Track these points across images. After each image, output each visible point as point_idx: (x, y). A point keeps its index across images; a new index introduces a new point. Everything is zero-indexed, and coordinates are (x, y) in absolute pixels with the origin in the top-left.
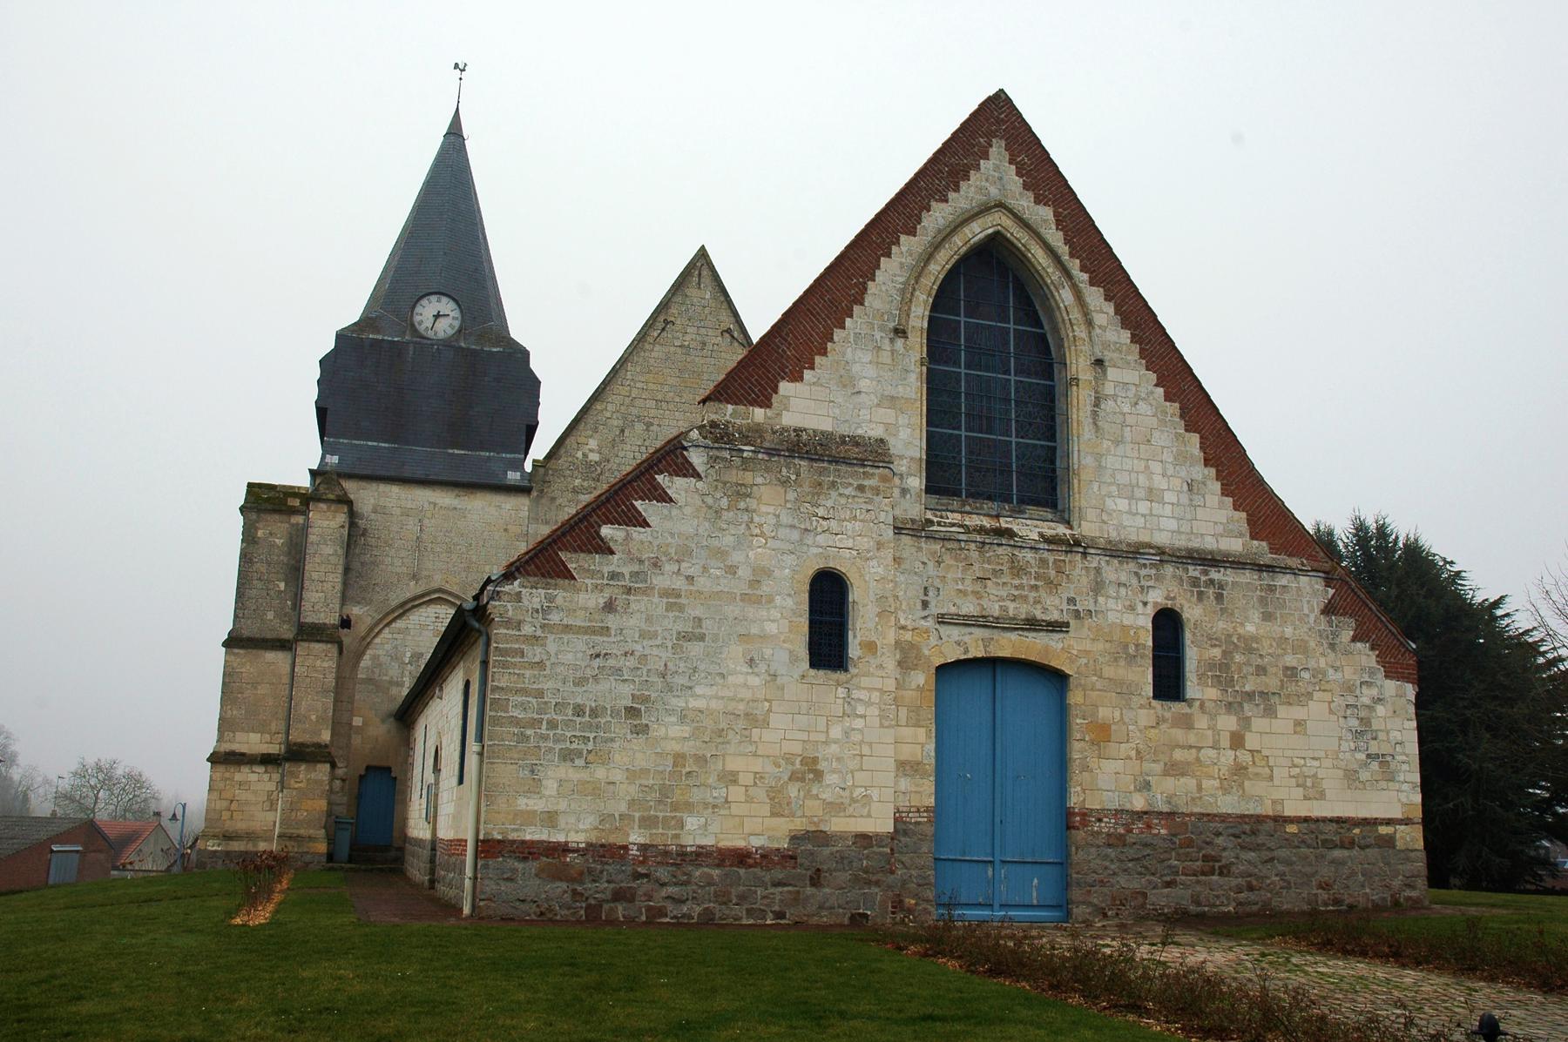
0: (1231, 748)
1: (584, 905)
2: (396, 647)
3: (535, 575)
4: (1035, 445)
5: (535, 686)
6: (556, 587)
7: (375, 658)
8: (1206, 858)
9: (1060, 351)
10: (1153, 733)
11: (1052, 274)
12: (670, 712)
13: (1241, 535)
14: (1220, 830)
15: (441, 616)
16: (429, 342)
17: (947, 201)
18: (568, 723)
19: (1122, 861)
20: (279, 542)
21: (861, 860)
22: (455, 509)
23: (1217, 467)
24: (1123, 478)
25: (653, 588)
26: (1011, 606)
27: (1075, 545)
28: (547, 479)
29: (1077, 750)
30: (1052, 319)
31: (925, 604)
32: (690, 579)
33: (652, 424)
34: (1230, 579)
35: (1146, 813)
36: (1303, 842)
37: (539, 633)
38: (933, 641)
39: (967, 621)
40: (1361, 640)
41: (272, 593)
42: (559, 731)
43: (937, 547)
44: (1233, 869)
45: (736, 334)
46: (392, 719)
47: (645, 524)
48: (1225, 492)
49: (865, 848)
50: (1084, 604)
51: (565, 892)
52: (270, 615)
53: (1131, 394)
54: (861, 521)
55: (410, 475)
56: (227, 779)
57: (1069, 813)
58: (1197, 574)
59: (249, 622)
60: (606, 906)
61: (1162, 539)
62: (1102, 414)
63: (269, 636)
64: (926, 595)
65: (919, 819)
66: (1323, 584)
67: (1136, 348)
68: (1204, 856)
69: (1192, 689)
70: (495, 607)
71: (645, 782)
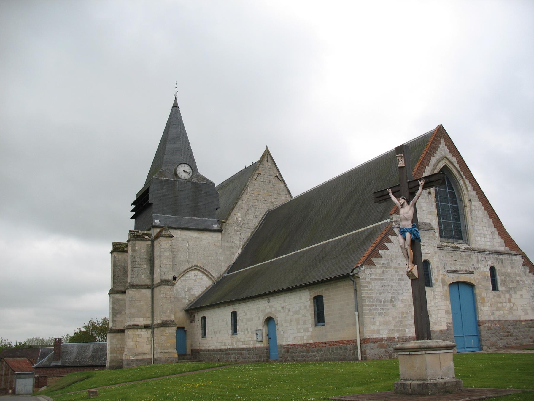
0: (509, 303)
1: (388, 354)
2: (183, 286)
3: (367, 265)
4: (456, 223)
5: (371, 295)
6: (372, 268)
7: (177, 290)
8: (508, 332)
9: (460, 197)
10: (493, 299)
11: (458, 176)
12: (399, 300)
13: (503, 246)
14: (509, 324)
15: (196, 275)
16: (183, 180)
17: (434, 156)
18: (379, 305)
19: (491, 334)
20: (143, 251)
21: (441, 337)
22: (198, 238)
23: (496, 228)
24: (478, 232)
25: (392, 267)
26: (462, 267)
27: (472, 250)
28: (226, 227)
29: (479, 305)
30: (457, 188)
31: (444, 268)
32: (399, 264)
33: (256, 208)
34: (504, 258)
35: (494, 321)
36: (526, 326)
37: (370, 281)
38: (447, 278)
39: (456, 272)
40: (530, 272)
41: (142, 268)
42: (378, 308)
43: (445, 252)
44: (513, 334)
45: (279, 177)
46: (184, 311)
47: (388, 249)
48: (499, 234)
49: (442, 334)
50: (476, 266)
51: (384, 351)
52: (142, 277)
53: (477, 208)
54: (431, 246)
55: (183, 227)
56: (134, 334)
57: (479, 322)
58: (497, 257)
59: (136, 279)
60: (393, 354)
61: (488, 247)
62: (472, 214)
63: (143, 284)
64: (444, 265)
65: (450, 326)
66: (521, 258)
67: (477, 196)
68: (507, 331)
69: (500, 287)
70: (360, 274)
71: (396, 320)
